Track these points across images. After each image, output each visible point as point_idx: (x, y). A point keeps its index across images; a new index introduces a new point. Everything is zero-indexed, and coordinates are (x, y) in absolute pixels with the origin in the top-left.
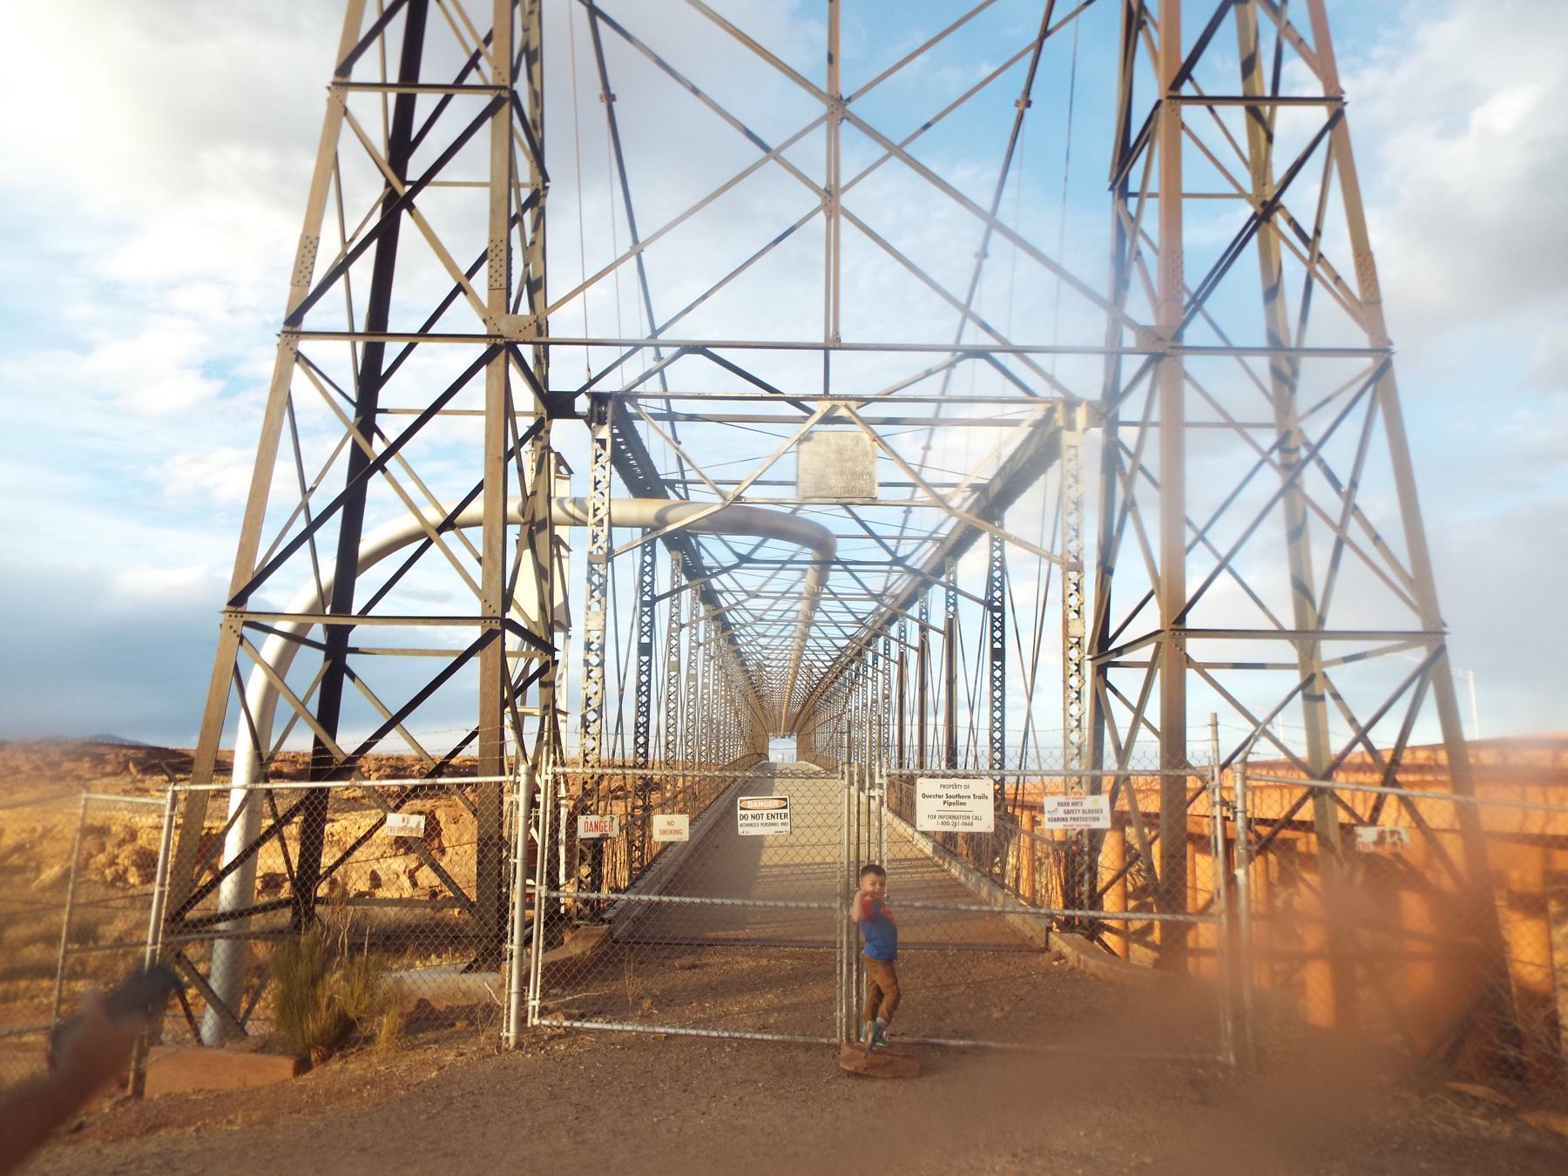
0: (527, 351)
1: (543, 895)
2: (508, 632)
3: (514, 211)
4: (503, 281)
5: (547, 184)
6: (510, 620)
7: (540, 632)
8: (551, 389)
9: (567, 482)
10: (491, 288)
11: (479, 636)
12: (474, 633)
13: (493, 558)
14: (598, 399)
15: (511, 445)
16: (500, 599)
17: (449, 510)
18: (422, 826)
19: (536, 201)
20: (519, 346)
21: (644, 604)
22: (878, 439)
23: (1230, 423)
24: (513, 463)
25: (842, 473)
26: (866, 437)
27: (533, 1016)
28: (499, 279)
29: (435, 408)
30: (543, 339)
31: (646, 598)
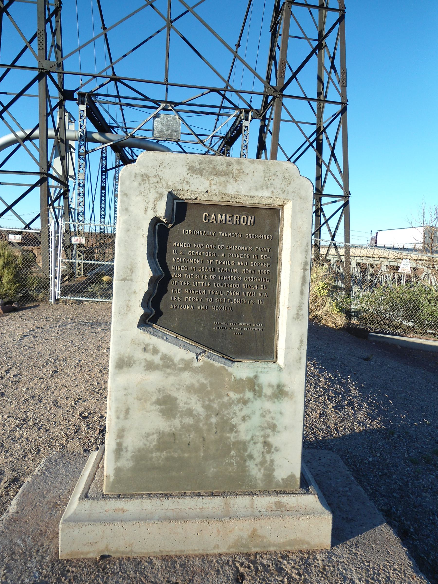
0: (55, 76)
1: (61, 260)
2: (49, 178)
3: (47, 17)
4: (44, 46)
5: (61, 5)
6: (50, 174)
7: (63, 179)
8: (65, 88)
9: (74, 124)
10: (39, 49)
11: (39, 179)
12: (37, 178)
13: (44, 150)
14: (82, 95)
15: (49, 110)
16: (46, 167)
17: (28, 132)
18: (21, 239)
19: (57, 12)
20: (51, 73)
21: (102, 172)
22: (181, 118)
23: (294, 121)
24: (50, 118)
25: (168, 130)
26: (177, 117)
27: (58, 296)
28: (42, 46)
29: (21, 93)
30: (61, 71)
31: (104, 169)
